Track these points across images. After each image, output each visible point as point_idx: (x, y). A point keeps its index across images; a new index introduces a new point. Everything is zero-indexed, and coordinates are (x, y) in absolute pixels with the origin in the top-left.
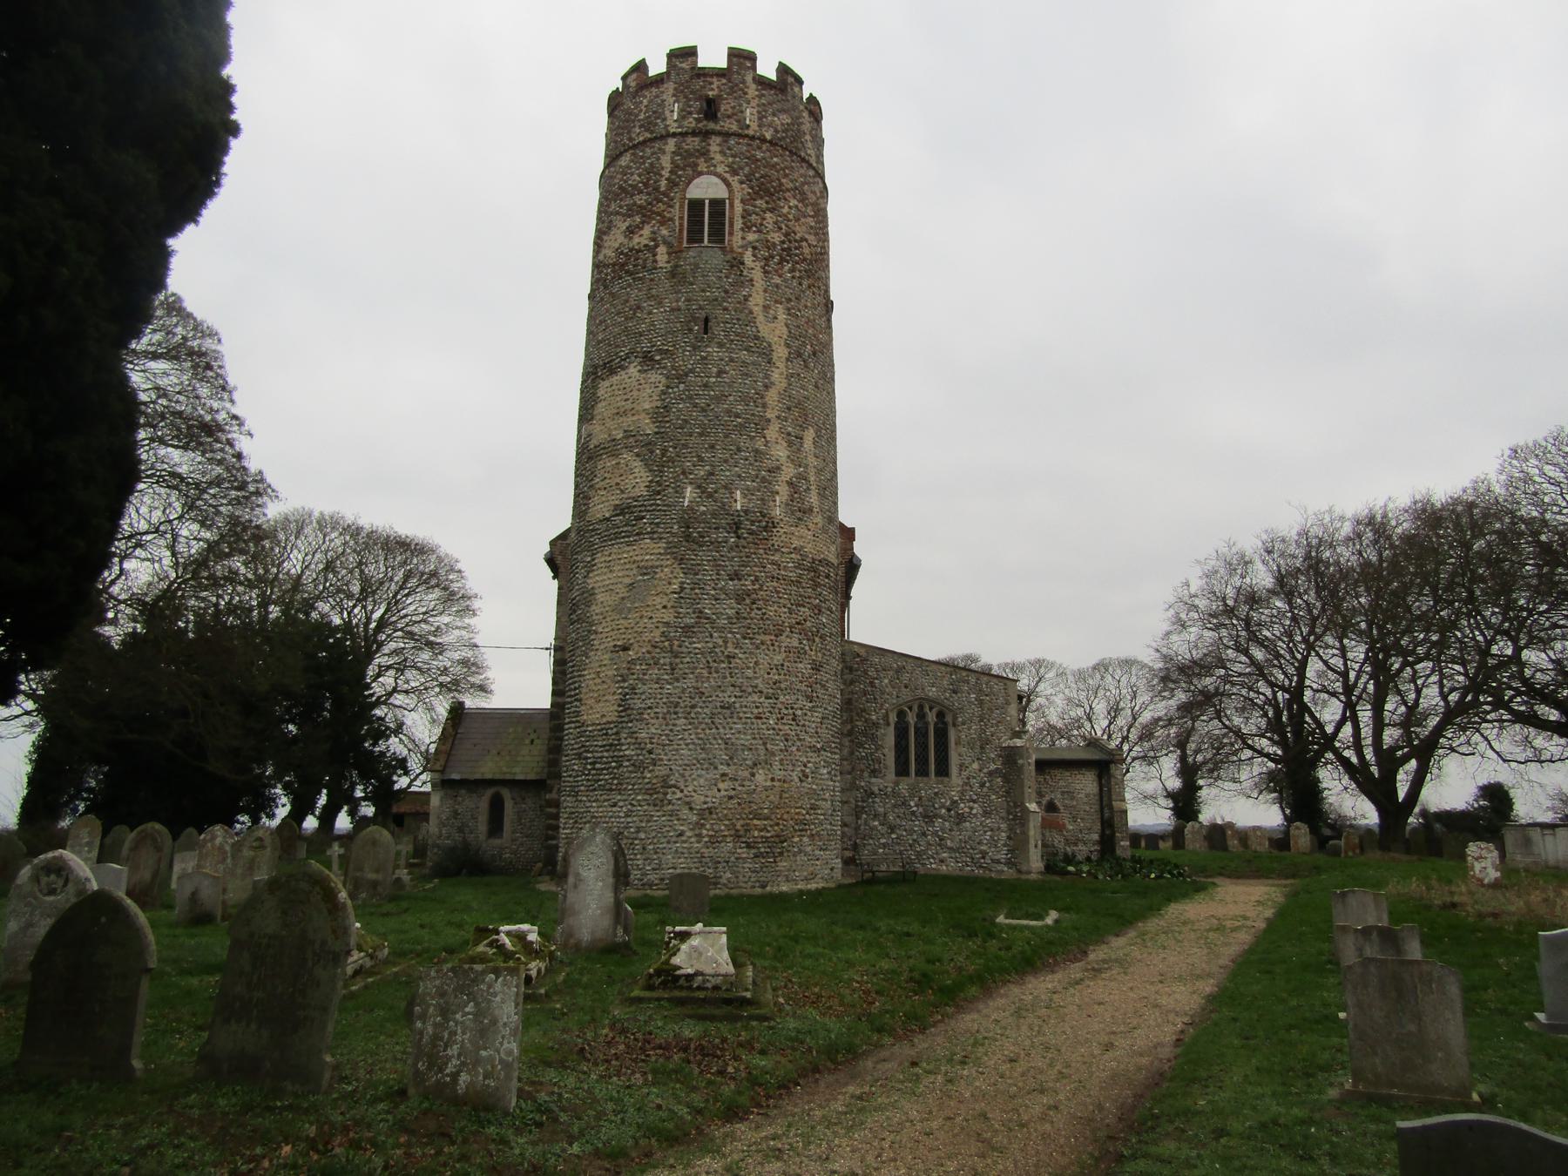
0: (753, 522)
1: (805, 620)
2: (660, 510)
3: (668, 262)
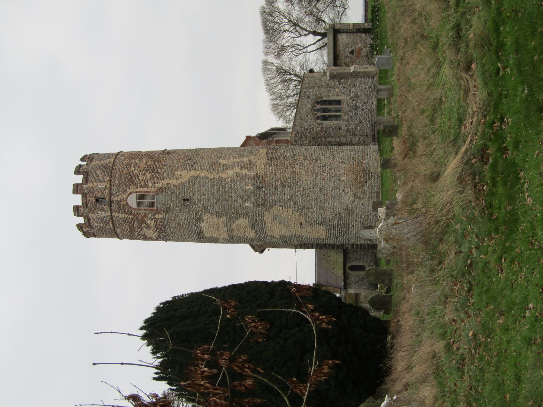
0: (257, 182)
1: (290, 163)
2: (254, 214)
3: (162, 214)
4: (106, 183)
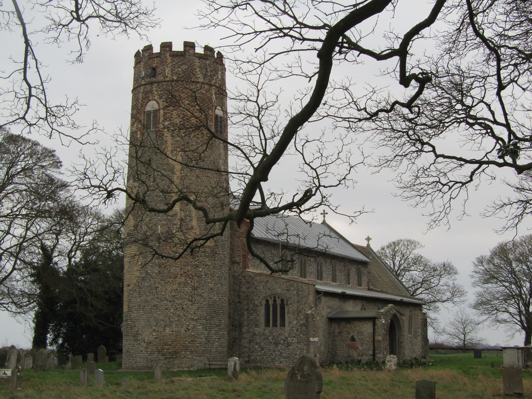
4: (170, 76)
